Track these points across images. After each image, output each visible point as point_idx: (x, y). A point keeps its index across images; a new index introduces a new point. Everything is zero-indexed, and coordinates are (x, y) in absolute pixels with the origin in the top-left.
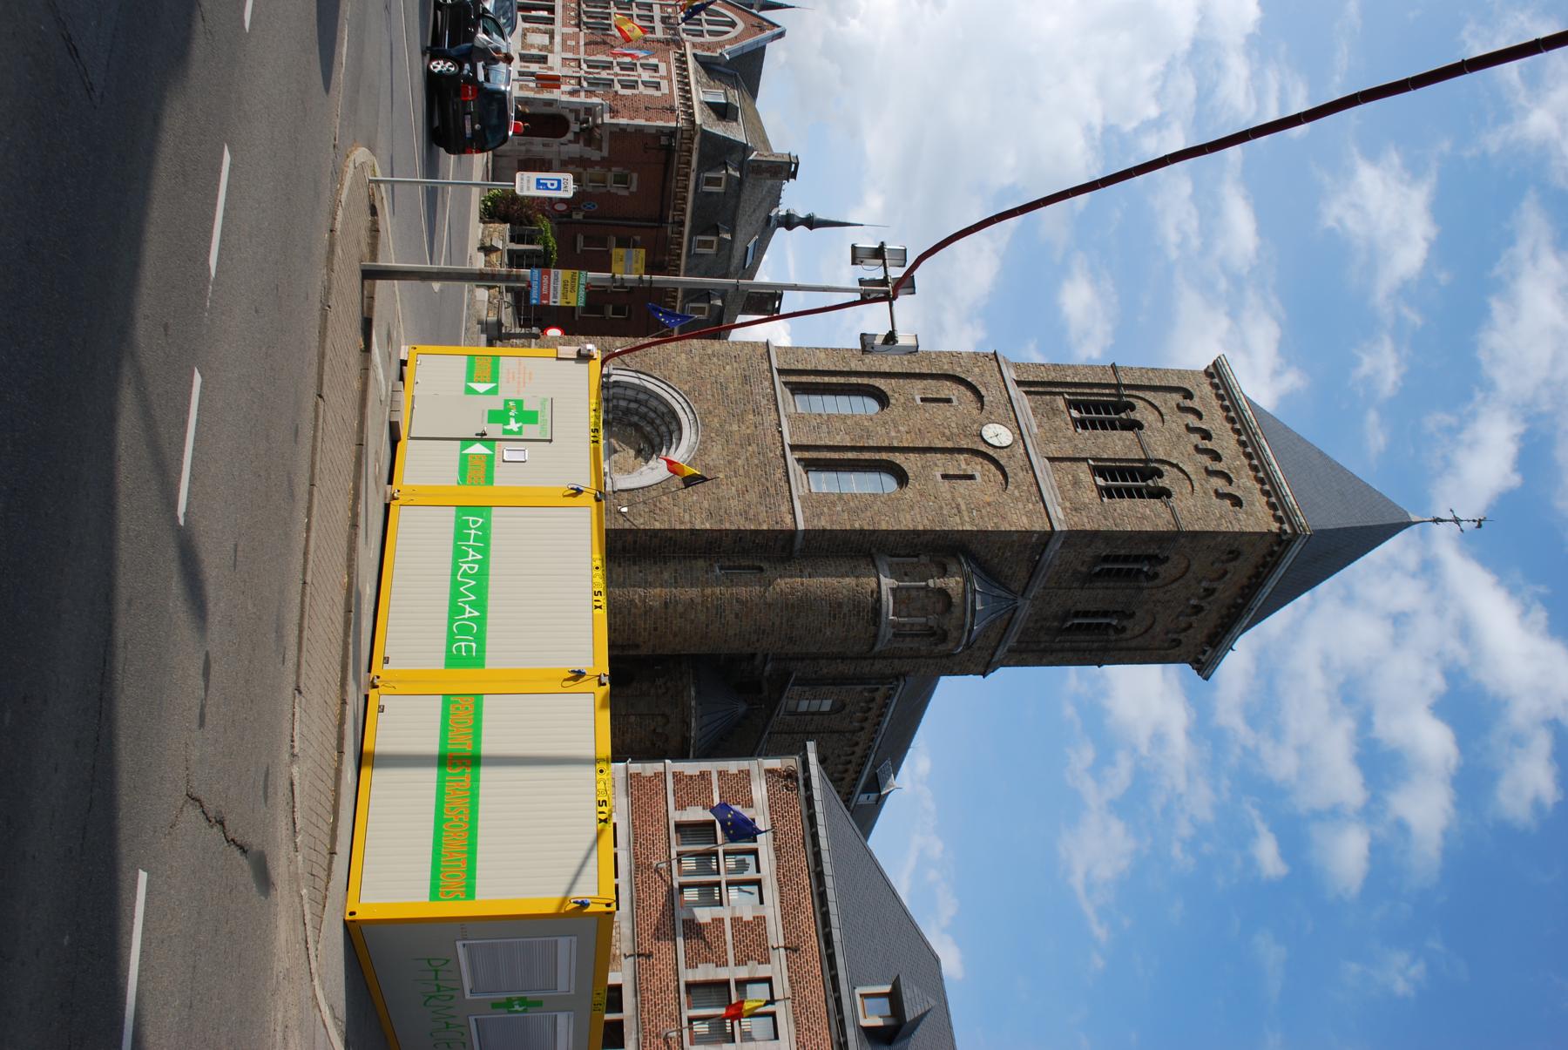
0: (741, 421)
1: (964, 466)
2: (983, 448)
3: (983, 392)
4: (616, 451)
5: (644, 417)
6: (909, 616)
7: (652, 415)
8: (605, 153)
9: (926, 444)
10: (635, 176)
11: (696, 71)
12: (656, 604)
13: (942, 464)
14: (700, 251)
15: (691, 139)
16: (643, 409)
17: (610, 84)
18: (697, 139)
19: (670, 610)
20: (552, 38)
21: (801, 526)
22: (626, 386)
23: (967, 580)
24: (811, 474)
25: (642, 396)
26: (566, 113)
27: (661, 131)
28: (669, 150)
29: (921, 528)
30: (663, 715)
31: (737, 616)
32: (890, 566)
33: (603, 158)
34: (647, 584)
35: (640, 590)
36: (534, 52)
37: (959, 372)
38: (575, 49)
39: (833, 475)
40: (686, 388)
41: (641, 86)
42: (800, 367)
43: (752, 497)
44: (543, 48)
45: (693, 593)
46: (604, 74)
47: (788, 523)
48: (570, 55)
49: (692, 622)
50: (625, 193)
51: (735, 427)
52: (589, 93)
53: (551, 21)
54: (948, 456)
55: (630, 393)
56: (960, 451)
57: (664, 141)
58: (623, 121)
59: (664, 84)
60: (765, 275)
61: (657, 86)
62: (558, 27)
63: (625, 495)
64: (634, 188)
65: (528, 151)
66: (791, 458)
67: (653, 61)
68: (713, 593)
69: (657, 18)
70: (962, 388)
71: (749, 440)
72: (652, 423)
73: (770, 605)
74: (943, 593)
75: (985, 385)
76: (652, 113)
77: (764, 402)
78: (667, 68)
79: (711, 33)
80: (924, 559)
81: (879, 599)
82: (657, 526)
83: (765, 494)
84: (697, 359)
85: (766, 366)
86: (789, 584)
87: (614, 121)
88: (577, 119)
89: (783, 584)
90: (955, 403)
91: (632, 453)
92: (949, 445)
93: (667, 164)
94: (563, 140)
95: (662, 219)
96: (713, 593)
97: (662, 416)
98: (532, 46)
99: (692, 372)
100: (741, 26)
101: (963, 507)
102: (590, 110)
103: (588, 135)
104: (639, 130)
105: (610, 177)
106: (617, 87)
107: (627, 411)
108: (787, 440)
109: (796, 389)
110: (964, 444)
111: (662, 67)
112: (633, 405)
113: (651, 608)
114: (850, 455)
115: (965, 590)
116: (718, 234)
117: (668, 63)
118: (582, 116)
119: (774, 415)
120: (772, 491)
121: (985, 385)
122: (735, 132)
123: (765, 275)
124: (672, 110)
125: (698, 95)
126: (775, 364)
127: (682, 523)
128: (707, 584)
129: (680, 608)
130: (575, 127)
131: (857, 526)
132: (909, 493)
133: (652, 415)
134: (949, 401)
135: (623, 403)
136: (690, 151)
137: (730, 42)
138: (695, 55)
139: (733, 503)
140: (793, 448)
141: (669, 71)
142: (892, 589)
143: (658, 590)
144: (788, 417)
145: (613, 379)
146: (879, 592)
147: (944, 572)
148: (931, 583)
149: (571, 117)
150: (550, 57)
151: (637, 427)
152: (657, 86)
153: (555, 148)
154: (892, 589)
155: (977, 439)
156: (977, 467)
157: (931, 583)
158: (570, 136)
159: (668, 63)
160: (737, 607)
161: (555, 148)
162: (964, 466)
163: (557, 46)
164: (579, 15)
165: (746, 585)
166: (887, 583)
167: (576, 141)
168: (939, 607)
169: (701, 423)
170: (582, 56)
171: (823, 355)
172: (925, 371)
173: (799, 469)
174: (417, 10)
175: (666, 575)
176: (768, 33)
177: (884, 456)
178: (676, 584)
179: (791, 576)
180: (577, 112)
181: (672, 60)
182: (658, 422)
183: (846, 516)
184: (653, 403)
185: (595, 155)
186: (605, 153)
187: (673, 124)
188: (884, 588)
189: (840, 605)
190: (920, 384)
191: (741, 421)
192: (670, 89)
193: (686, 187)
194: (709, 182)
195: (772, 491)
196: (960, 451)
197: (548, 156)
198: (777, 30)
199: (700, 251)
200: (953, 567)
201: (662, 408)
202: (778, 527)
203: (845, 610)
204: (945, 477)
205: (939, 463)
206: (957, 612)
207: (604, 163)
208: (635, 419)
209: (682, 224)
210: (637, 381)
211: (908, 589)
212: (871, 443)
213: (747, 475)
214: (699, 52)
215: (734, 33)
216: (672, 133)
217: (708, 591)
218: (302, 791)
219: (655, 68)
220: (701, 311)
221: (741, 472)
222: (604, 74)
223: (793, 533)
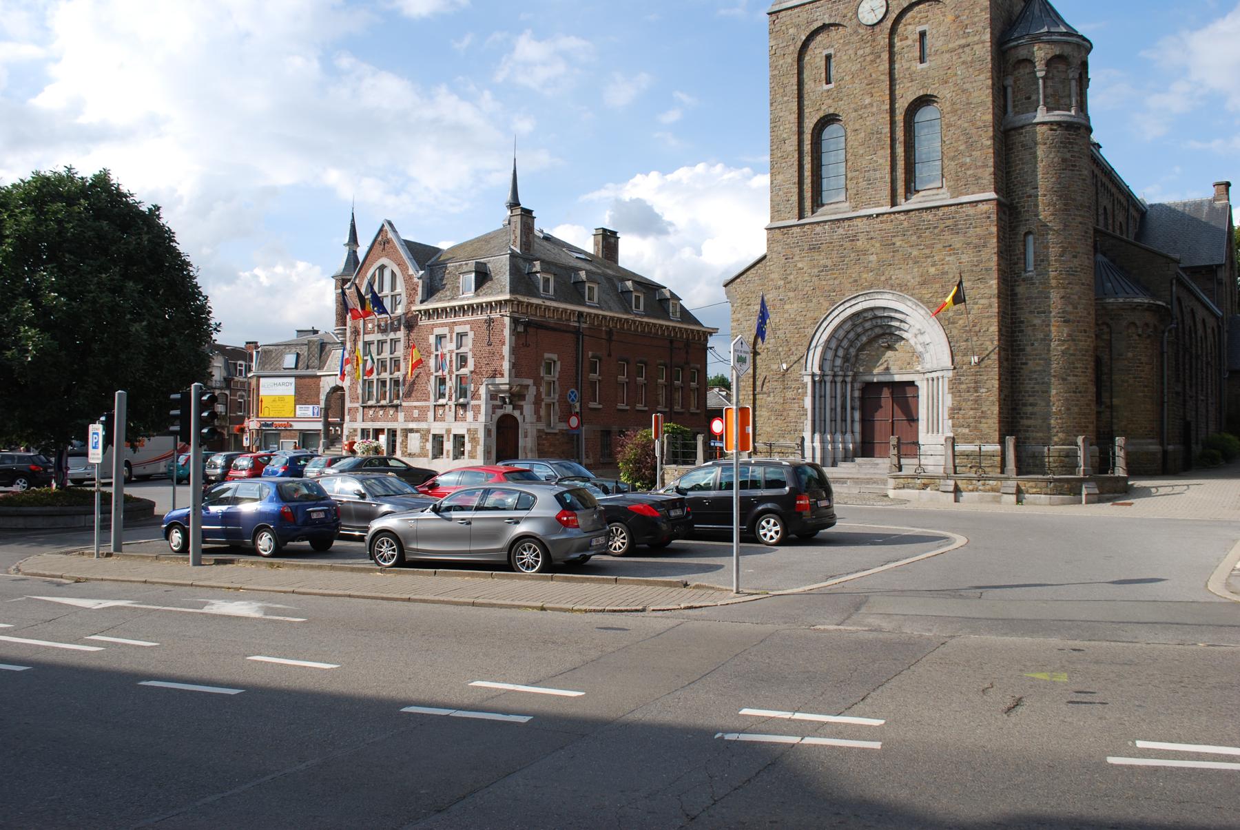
0: (865, 252)
1: (909, 42)
2: (888, 23)
3: (819, 24)
4: (887, 369)
5: (852, 344)
6: (1069, 96)
7: (852, 335)
8: (530, 382)
9: (887, 78)
10: (547, 355)
11: (440, 300)
12: (1066, 331)
13: (907, 62)
14: (596, 300)
15: (520, 303)
16: (845, 343)
17: (461, 378)
18: (521, 298)
19: (1072, 317)
20: (411, 431)
21: (993, 195)
22: (823, 359)
23: (1037, 39)
24: (825, 201)
25: (833, 345)
26: (496, 417)
27: (513, 331)
28: (527, 325)
29: (989, 82)
30: (1128, 327)
31: (1075, 257)
32: (1017, 113)
33: (535, 384)
34: (1047, 339)
35: (1053, 345)
36: (429, 446)
37: (794, 49)
38: (423, 410)
39: (825, 182)
40: (826, 304)
41: (383, 356)
42: (795, 198)
43: (957, 241)
44: (424, 438)
45: (1055, 296)
46: (451, 384)
47: (992, 207)
48: (431, 414)
49: (1080, 298)
50: (559, 364)
51: (873, 258)
52: (475, 395)
53: (392, 433)
54: (897, 57)
55: (830, 355)
56: (891, 45)
57: (520, 329)
58: (506, 366)
59: (458, 329)
60: (589, 245)
61: (461, 336)
62: (399, 424)
63: (957, 359)
64: (555, 357)
65: (532, 451)
66: (904, 206)
67: (432, 339)
68: (1055, 278)
69: (380, 337)
70: (812, 45)
71: (888, 245)
72: (858, 336)
73: (1066, 226)
74: (1049, 63)
75: (809, 23)
76: (494, 339)
77: (841, 231)
78: (440, 326)
79: (393, 288)
80: (1010, 81)
81: (1059, 123)
82: (994, 328)
83: (954, 229)
84: (791, 294)
85: (797, 230)
86: (1045, 207)
87: (506, 374)
88: (501, 407)
89: (1045, 212)
90: (831, 51)
91: (889, 353)
92: (885, 56)
93: (539, 326)
94: (520, 419)
95: (577, 332)
96: (1055, 278)
97: (855, 326)
98: (423, 448)
99: (807, 298)
100: (384, 261)
101: (963, 42)
102: (492, 396)
103: (516, 397)
104: (514, 351)
105: (547, 378)
106: (463, 371)
107: (846, 359)
108: (887, 209)
109: (817, 203)
110: (883, 40)
111: (438, 331)
112: (841, 353)
113: (1069, 335)
114: (900, 150)
115: (1048, 42)
116: (583, 282)
117: (434, 326)
118: (498, 403)
119: (855, 222)
120: (949, 223)
121: (809, 23)
122: (500, 265)
123: (589, 245)
124: (490, 322)
125: (468, 297)
126: (795, 221)
127: (990, 306)
128: (1046, 283)
129: (1069, 308)
130: (508, 409)
131: (989, 142)
132: (945, 93)
133: (852, 335)
134: (828, 58)
135: (839, 362)
136: (529, 304)
137: (403, 268)
138: (422, 302)
139: (965, 258)
140: (801, 216)
141: (443, 325)
142: (1049, 110)
143: (1053, 329)
144: (855, 208)
145: (817, 371)
146: (1051, 123)
147: (1030, 62)
148: (1040, 74)
149: (500, 412)
150: (433, 432)
151: (862, 348)
152: (461, 336)
153: (528, 427)
154: (1049, 110)
155: (877, 29)
156: (910, 29)
157: (1040, 74)
158: (517, 414)
159: (434, 326)
160: (1067, 256)
161: (528, 427)
162: (909, 42)
163: (423, 425)
164: (382, 407)
165: (1047, 247)
166: (1041, 115)
167: (521, 408)
168: (1062, 67)
169: (870, 288)
170: (432, 403)
171: (780, 178)
172: (795, 80)
173: (820, 210)
174: (897, 547)
175: (1037, 321)
176: (390, 235)
177: (900, 118)
178: (1047, 312)
179: (1036, 206)
180: (495, 408)
181: (431, 322)
182: (860, 330)
183: (976, 154)
184: (841, 333)
185: (532, 391)
186: (530, 382)
187: (507, 320)
188: (1047, 119)
189: (1064, 160)
190: (809, 85)
191: (865, 252)
192: (464, 324)
193: (556, 309)
194: (546, 289)
195: (949, 223)
196: (891, 45)
197: (535, 433)
198: (387, 227)
199: (596, 300)
200: (1022, 53)
201: (847, 326)
202: (994, 217)
203: (1068, 156)
204: (922, 60)
205: (906, 65)
206: (1067, 50)
207: (537, 384)
208: (853, 351)
209: (581, 314)
210: (819, 349)
211: (1045, 97)
212: (887, 130)
213: (931, 246)
214: (419, 297)
215: (392, 266)
216: (515, 321)
217: (1053, 282)
218: (688, 617)
219: (440, 338)
220: (637, 298)
221: (927, 251)
222: (451, 384)
223: (999, 204)
